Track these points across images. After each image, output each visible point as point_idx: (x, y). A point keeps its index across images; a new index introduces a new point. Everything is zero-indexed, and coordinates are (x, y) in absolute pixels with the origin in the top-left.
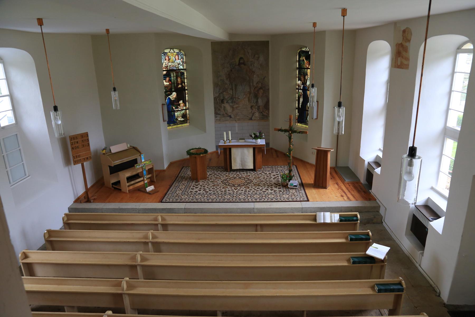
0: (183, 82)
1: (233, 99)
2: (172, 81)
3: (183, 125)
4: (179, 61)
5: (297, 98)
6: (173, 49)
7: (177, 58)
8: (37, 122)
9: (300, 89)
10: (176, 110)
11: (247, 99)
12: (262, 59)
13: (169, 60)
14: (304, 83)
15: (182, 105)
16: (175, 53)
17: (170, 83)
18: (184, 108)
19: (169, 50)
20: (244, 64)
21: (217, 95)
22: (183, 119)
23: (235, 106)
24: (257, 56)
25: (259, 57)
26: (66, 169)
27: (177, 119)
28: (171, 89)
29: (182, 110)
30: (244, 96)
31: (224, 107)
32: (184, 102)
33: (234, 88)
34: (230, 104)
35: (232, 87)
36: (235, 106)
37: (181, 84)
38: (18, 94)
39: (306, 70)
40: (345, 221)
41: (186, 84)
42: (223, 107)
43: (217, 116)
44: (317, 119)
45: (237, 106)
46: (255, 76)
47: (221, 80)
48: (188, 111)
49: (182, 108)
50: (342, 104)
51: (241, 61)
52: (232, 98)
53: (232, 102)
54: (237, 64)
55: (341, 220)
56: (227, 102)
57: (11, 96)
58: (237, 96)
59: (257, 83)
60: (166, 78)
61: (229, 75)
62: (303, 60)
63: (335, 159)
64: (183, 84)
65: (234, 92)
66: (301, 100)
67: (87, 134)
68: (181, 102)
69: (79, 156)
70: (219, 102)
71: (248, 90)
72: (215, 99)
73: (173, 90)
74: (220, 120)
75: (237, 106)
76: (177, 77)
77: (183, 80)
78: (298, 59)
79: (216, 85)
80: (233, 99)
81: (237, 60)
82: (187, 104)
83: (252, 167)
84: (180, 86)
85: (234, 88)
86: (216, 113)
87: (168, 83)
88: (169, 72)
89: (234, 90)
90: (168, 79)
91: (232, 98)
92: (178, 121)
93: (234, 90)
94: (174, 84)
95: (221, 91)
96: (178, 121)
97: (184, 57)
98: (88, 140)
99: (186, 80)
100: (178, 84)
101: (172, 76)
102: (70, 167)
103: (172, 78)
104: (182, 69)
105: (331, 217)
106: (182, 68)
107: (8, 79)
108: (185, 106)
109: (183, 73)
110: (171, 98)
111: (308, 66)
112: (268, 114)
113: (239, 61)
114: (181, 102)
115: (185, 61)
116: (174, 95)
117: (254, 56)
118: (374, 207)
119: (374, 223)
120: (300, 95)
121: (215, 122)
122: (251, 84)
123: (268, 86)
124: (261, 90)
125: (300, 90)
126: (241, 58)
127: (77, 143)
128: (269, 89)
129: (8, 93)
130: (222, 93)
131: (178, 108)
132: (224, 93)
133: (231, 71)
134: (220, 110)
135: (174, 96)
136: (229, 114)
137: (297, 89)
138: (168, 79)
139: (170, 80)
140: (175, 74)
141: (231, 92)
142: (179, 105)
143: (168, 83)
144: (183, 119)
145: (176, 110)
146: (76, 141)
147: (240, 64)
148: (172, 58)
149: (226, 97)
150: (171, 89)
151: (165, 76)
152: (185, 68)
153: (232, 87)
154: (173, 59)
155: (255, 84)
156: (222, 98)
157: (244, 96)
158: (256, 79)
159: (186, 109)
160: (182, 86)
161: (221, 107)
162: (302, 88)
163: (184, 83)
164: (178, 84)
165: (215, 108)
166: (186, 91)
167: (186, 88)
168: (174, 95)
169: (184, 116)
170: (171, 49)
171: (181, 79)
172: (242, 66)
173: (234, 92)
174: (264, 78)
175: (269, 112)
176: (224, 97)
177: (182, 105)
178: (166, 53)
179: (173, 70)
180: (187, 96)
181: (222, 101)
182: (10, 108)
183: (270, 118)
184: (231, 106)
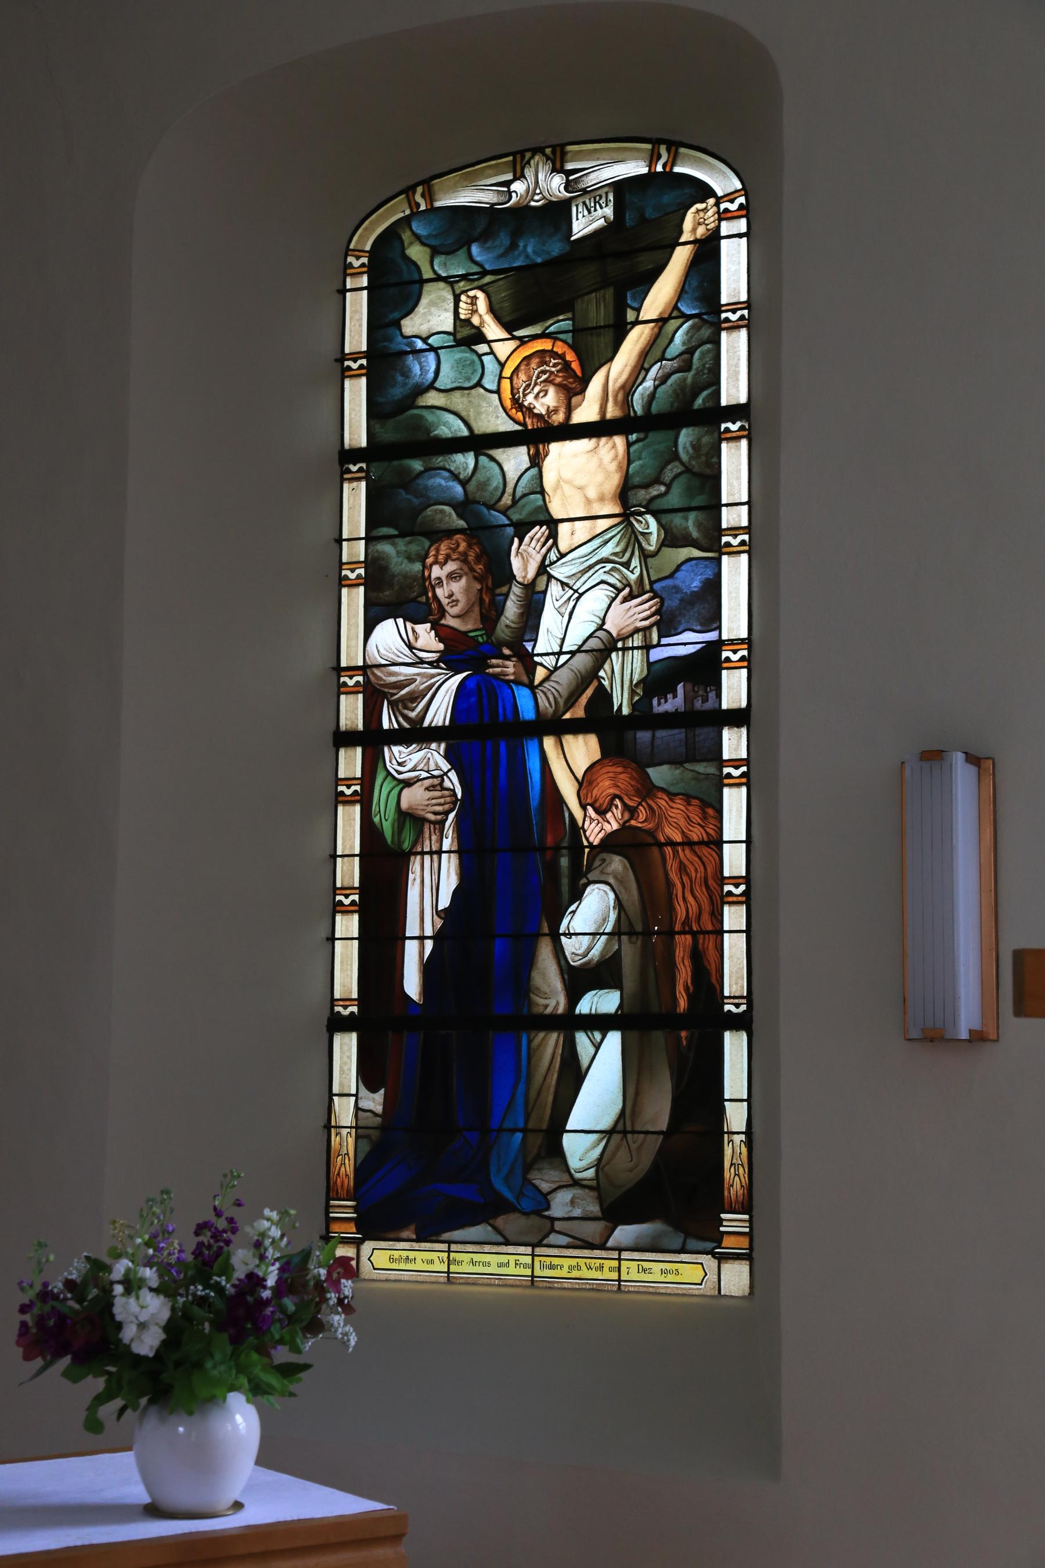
5: (349, 872)
9: (417, 734)
14: (486, 648)
39: (514, 460)
62: (468, 336)
66: (433, 885)
78: (357, 337)
111: (546, 402)
120: (408, 818)
125: (403, 758)
137: (345, 739)
162: (439, 711)
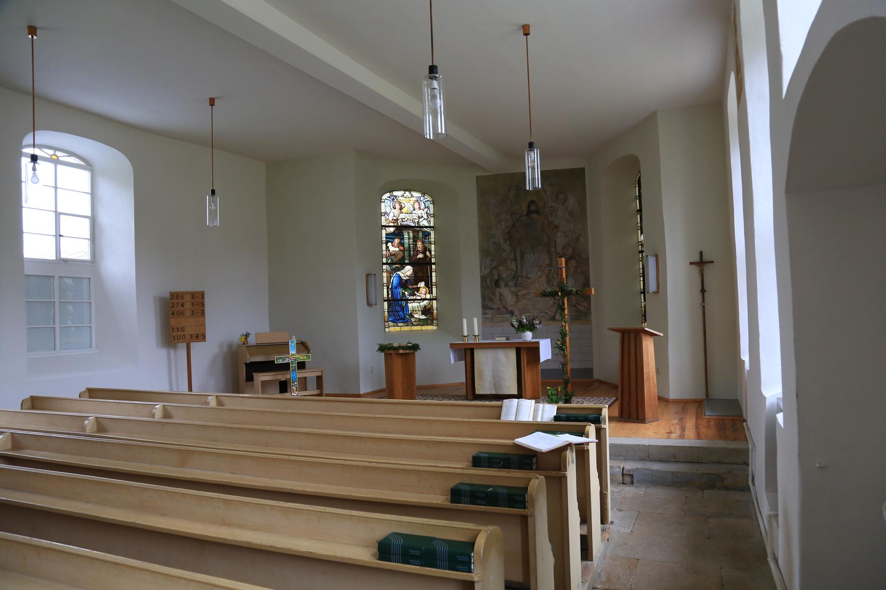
0: (425, 250)
1: (516, 278)
2: (406, 246)
3: (424, 328)
4: (419, 212)
6: (410, 191)
7: (417, 206)
8: (121, 263)
10: (411, 297)
11: (544, 279)
12: (572, 202)
13: (401, 209)
15: (423, 290)
16: (414, 199)
17: (402, 248)
18: (428, 296)
19: (402, 193)
20: (537, 212)
21: (487, 272)
22: (423, 317)
23: (520, 293)
24: (561, 196)
25: (565, 199)
26: (163, 352)
27: (411, 316)
28: (403, 258)
29: (424, 300)
30: (539, 273)
31: (500, 294)
32: (429, 285)
33: (518, 259)
34: (513, 289)
35: (515, 257)
36: (520, 293)
37: (424, 252)
38: (104, 218)
40: (568, 419)
41: (433, 253)
42: (498, 295)
43: (487, 311)
44: (658, 292)
45: (525, 292)
46: (559, 234)
47: (494, 243)
48: (435, 302)
49: (423, 296)
50: (535, 145)
51: (533, 208)
52: (515, 277)
53: (516, 285)
54: (525, 213)
55: (556, 418)
56: (506, 285)
57: (94, 221)
58: (524, 274)
59: (563, 248)
60: (393, 239)
61: (509, 233)
63: (703, 381)
64: (428, 253)
65: (519, 266)
67: (202, 295)
68: (422, 284)
69: (183, 329)
70: (490, 285)
71: (547, 262)
72: (483, 279)
73: (407, 261)
74: (492, 319)
75: (525, 292)
76: (415, 239)
77: (426, 245)
79: (485, 253)
80: (516, 278)
81: (524, 206)
82: (434, 289)
83: (515, 391)
84: (420, 256)
85: (518, 259)
86: (485, 307)
87: (397, 249)
88: (400, 230)
89: (519, 261)
90: (397, 241)
91: (515, 277)
92: (413, 320)
93: (519, 261)
94: (410, 251)
95: (495, 264)
96: (413, 320)
97: (431, 206)
98: (203, 305)
99: (433, 246)
100: (418, 252)
101: (406, 236)
102: (172, 352)
103: (406, 241)
104: (426, 227)
105: (536, 411)
106: (427, 224)
107: (93, 194)
108: (431, 292)
109: (430, 234)
110: (402, 275)
112: (589, 309)
113: (529, 207)
114: (422, 284)
115: (432, 212)
116: (408, 271)
117: (557, 196)
118: (736, 452)
119: (727, 488)
121: (483, 322)
122: (553, 250)
123: (587, 252)
124: (573, 262)
126: (532, 202)
127: (182, 305)
128: (587, 259)
129: (89, 214)
130: (495, 267)
131: (414, 295)
132: (501, 268)
133: (514, 226)
134: (491, 300)
135: (409, 273)
136: (510, 309)
138: (397, 241)
139: (401, 244)
140: (411, 235)
141: (513, 266)
142: (418, 289)
143: (397, 249)
144: (423, 317)
145: (411, 297)
146: (180, 301)
147: (529, 212)
148: (408, 207)
149: (504, 276)
150: (403, 258)
151: (390, 237)
152: (432, 224)
153: (515, 257)
154: (407, 207)
155: (559, 250)
156: (496, 277)
157: (539, 273)
158: (561, 240)
159: (430, 300)
160: (426, 256)
161: (494, 293)
163: (430, 251)
164: (418, 252)
165: (484, 297)
166: (433, 267)
167: (433, 260)
168: (408, 271)
169: (426, 311)
170: (405, 190)
171: (423, 243)
172: (534, 216)
173: (519, 266)
174: (577, 239)
175: (589, 304)
176: (499, 275)
177: (423, 290)
178: (396, 196)
179: (408, 227)
180: (434, 274)
181: (497, 284)
182: (88, 235)
183: (593, 317)
184: (513, 292)
